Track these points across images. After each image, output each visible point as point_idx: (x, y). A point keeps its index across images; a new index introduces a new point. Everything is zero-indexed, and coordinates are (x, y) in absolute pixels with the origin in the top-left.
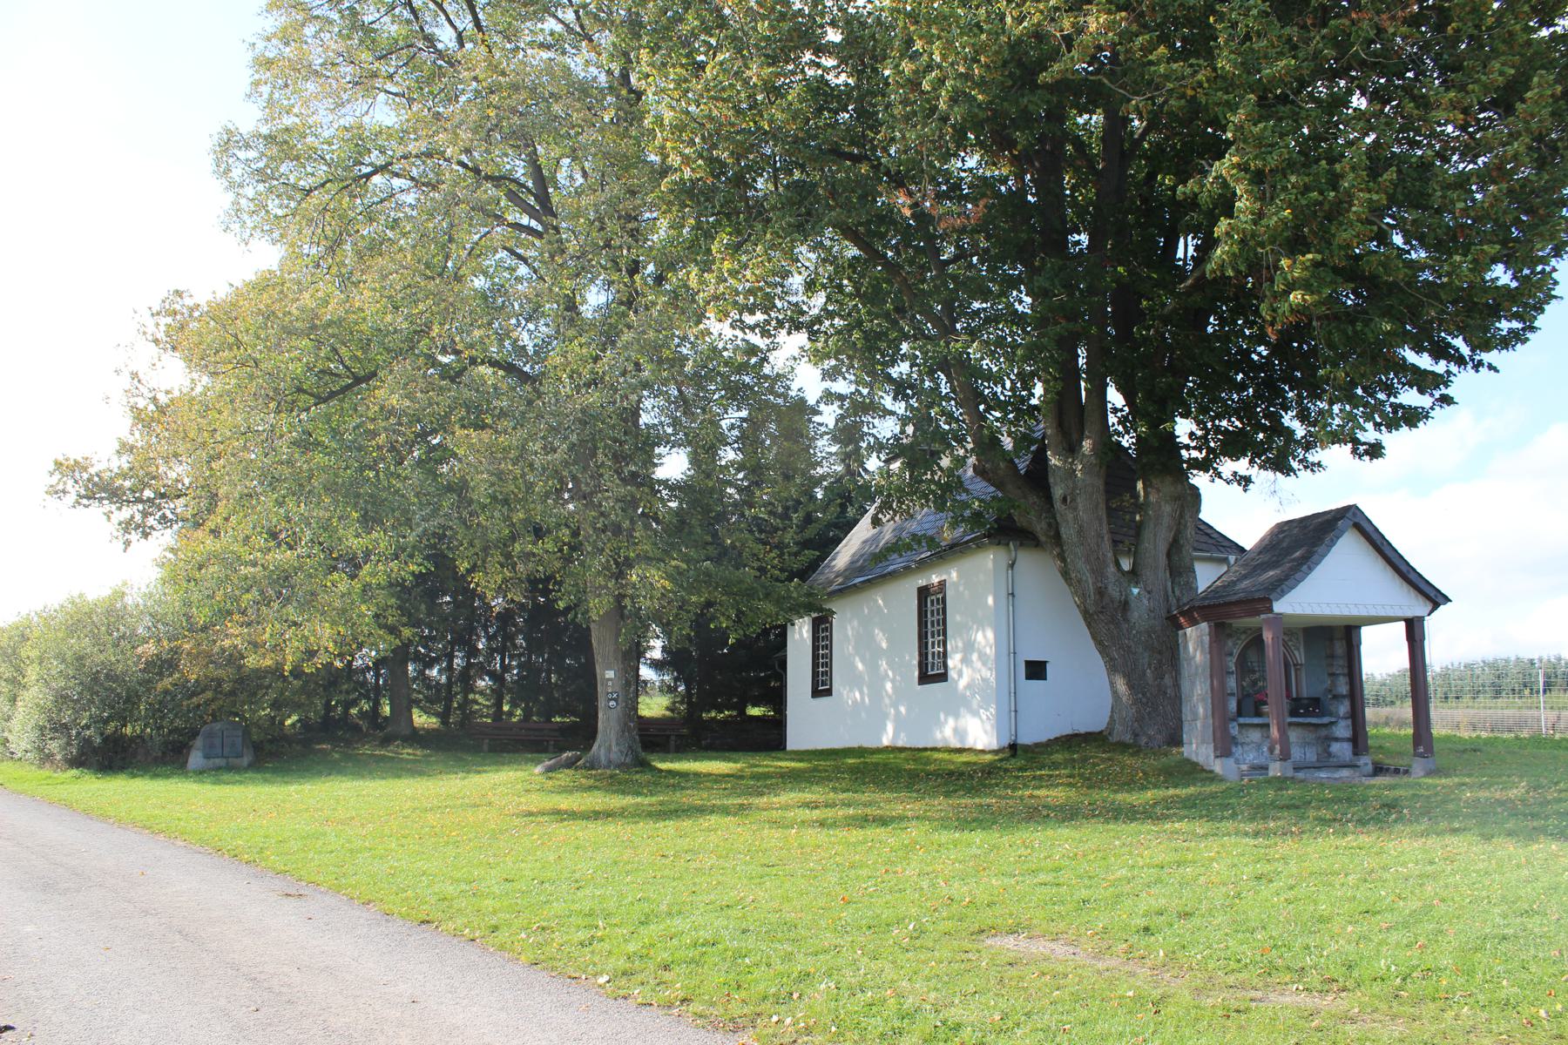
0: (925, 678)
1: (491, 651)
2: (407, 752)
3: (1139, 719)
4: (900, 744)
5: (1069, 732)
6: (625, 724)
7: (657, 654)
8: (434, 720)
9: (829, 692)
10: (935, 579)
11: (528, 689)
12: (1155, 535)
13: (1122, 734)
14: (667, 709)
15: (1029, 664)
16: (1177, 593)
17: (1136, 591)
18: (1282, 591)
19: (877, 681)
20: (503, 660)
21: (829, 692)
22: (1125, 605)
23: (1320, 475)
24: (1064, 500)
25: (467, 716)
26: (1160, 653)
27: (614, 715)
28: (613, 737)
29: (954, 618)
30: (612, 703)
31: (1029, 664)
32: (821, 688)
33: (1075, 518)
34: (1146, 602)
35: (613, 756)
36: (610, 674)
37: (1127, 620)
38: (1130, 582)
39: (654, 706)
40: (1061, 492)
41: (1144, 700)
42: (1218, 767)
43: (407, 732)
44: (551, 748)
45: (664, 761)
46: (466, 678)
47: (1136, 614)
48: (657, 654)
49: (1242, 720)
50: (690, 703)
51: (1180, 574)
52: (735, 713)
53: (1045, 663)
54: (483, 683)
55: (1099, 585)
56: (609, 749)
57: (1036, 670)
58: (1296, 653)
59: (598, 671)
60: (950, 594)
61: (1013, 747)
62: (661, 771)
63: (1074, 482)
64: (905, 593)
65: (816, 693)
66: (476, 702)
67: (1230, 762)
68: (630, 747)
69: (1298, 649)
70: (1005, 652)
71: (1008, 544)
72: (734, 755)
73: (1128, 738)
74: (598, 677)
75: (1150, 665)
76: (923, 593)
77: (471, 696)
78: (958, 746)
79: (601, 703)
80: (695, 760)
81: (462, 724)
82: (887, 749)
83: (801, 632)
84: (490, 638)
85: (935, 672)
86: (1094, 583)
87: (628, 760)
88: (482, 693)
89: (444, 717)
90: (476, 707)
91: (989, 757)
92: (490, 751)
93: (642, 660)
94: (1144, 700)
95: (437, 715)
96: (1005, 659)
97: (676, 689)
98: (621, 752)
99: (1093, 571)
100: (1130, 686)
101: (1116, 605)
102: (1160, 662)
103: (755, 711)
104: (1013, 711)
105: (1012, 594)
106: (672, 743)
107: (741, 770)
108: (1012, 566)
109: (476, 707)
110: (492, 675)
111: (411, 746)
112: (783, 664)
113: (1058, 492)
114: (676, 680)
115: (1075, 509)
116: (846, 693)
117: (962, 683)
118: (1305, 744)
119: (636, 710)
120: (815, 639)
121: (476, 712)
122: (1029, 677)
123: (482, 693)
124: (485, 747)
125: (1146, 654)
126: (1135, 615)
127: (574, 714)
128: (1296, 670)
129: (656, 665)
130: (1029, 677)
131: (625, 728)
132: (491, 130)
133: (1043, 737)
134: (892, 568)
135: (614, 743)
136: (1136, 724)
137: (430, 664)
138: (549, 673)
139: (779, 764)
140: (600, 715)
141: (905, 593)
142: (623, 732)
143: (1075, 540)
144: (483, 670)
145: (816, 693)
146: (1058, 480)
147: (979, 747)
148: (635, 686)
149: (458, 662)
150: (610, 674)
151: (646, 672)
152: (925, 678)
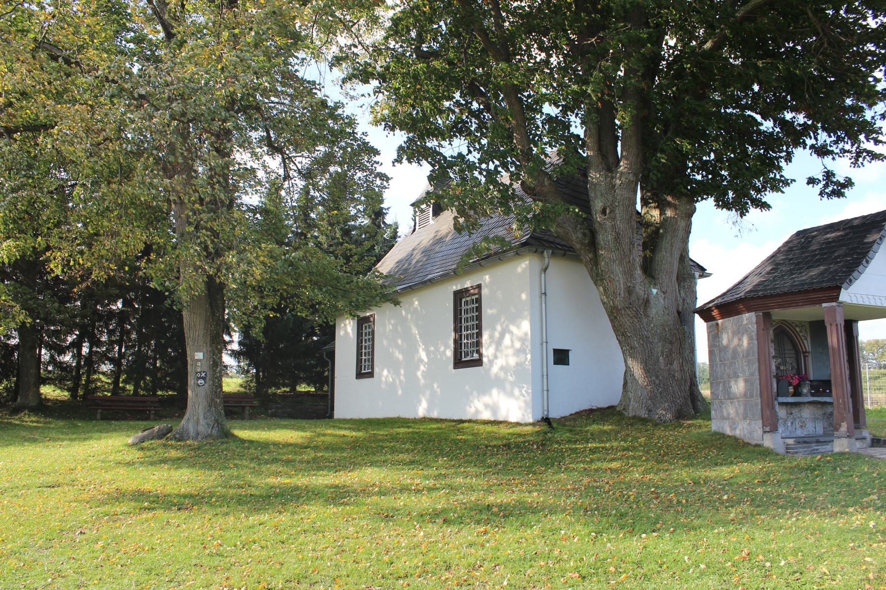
0: (459, 362)
1: (111, 343)
2: (29, 420)
3: (652, 398)
4: (435, 415)
5: (587, 407)
6: (212, 400)
7: (235, 347)
8: (66, 393)
9: (371, 375)
10: (468, 284)
11: (136, 371)
12: (672, 245)
13: (635, 409)
14: (241, 386)
15: (556, 351)
16: (683, 294)
17: (655, 291)
18: (851, 281)
19: (412, 363)
20: (120, 349)
21: (371, 375)
22: (647, 302)
23: (765, 213)
24: (604, 212)
25: (90, 392)
26: (671, 343)
27: (202, 391)
28: (201, 411)
29: (487, 312)
30: (201, 381)
31: (556, 351)
32: (364, 371)
33: (614, 227)
34: (662, 300)
35: (201, 429)
36: (199, 356)
37: (647, 316)
38: (650, 283)
39: (232, 384)
40: (601, 204)
41: (657, 382)
42: (768, 442)
43: (34, 404)
44: (152, 416)
45: (242, 428)
46: (91, 363)
47: (654, 311)
48: (235, 347)
49: (781, 399)
50: (258, 382)
51: (684, 280)
52: (288, 390)
53: (568, 351)
54: (106, 367)
55: (629, 284)
56: (197, 422)
57: (561, 357)
58: (805, 342)
59: (188, 353)
60: (485, 292)
61: (547, 420)
62: (243, 441)
63: (613, 196)
64: (442, 297)
65: (360, 375)
66: (100, 379)
67: (777, 436)
68: (216, 421)
69: (806, 339)
70: (538, 342)
71: (542, 253)
72: (304, 423)
73: (643, 414)
74: (189, 359)
75: (662, 353)
76: (459, 296)
77: (95, 377)
78: (492, 419)
79: (191, 381)
80: (270, 429)
81: (84, 397)
82: (425, 420)
83: (346, 329)
84: (111, 333)
85: (468, 358)
86: (625, 283)
87: (214, 432)
88: (104, 373)
89: (73, 391)
90: (99, 384)
91: (529, 429)
92: (102, 419)
93: (224, 352)
94: (657, 382)
95: (68, 390)
96: (539, 346)
97: (248, 371)
98: (208, 425)
99: (625, 273)
100: (647, 370)
101: (641, 301)
102: (671, 350)
103: (303, 388)
104: (545, 391)
105: (545, 293)
106: (247, 412)
107: (311, 439)
108: (545, 270)
109: (99, 384)
110: (112, 360)
111: (36, 415)
112: (332, 355)
113: (598, 205)
114: (249, 365)
115: (614, 219)
116: (383, 373)
117: (495, 369)
118: (815, 419)
119: (221, 386)
120: (359, 334)
121: (96, 388)
122: (556, 363)
123: (104, 373)
124: (98, 416)
125: (660, 344)
126: (653, 312)
127: (173, 389)
128: (805, 357)
129: (235, 354)
130: (556, 363)
131: (211, 404)
132: (118, 22)
133: (566, 412)
134: (430, 277)
135: (201, 417)
136: (649, 402)
137: (62, 351)
138: (155, 360)
139: (342, 432)
140: (190, 392)
141: (442, 297)
142: (210, 406)
143: (612, 246)
144: (104, 357)
145: (360, 375)
146: (599, 194)
147: (513, 419)
148: (217, 369)
149: (85, 350)
150: (199, 356)
151: (227, 359)
152: (459, 362)
